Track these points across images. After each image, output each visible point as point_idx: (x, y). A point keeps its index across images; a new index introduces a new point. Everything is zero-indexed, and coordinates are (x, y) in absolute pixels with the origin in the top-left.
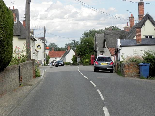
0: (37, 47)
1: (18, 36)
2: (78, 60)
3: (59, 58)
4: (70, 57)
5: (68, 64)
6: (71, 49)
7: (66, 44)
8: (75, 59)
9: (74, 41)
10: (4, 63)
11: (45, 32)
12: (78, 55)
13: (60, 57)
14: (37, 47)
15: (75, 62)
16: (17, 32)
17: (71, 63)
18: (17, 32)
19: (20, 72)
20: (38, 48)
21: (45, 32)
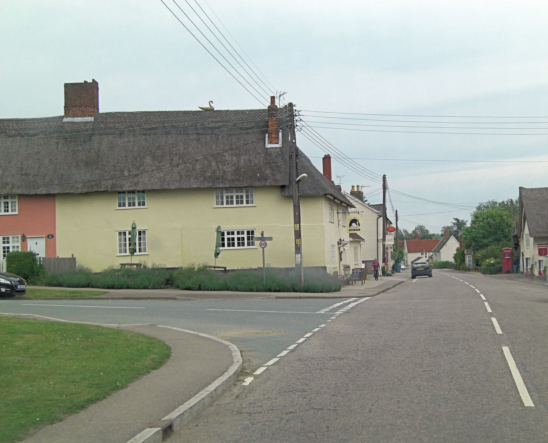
0: (350, 225)
1: (283, 187)
2: (468, 260)
3: (427, 253)
4: (449, 251)
5: (445, 265)
6: (450, 235)
7: (421, 228)
8: (460, 256)
9: (456, 219)
10: (225, 156)
11: (385, 188)
12: (468, 247)
13: (430, 252)
14: (350, 225)
15: (459, 264)
16: (279, 177)
17: (453, 265)
18: (279, 177)
19: (61, 280)
20: (352, 228)
21: (385, 188)
